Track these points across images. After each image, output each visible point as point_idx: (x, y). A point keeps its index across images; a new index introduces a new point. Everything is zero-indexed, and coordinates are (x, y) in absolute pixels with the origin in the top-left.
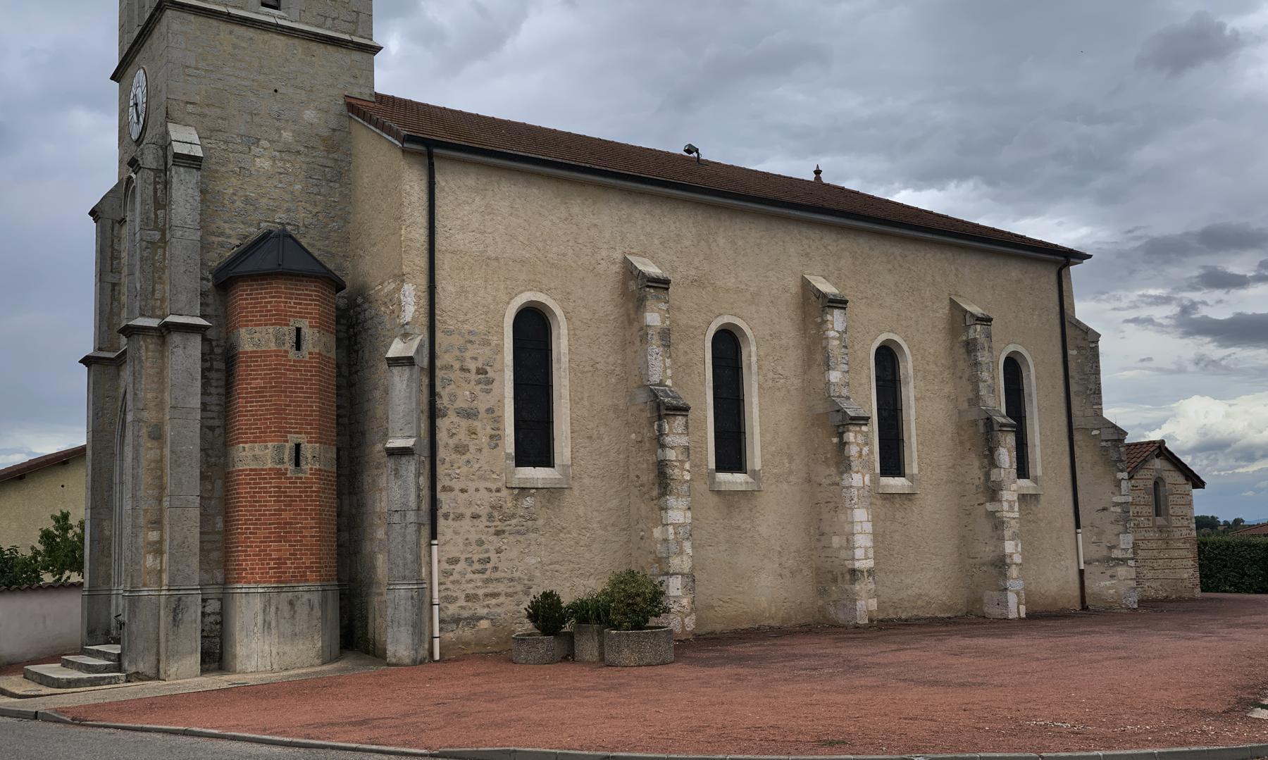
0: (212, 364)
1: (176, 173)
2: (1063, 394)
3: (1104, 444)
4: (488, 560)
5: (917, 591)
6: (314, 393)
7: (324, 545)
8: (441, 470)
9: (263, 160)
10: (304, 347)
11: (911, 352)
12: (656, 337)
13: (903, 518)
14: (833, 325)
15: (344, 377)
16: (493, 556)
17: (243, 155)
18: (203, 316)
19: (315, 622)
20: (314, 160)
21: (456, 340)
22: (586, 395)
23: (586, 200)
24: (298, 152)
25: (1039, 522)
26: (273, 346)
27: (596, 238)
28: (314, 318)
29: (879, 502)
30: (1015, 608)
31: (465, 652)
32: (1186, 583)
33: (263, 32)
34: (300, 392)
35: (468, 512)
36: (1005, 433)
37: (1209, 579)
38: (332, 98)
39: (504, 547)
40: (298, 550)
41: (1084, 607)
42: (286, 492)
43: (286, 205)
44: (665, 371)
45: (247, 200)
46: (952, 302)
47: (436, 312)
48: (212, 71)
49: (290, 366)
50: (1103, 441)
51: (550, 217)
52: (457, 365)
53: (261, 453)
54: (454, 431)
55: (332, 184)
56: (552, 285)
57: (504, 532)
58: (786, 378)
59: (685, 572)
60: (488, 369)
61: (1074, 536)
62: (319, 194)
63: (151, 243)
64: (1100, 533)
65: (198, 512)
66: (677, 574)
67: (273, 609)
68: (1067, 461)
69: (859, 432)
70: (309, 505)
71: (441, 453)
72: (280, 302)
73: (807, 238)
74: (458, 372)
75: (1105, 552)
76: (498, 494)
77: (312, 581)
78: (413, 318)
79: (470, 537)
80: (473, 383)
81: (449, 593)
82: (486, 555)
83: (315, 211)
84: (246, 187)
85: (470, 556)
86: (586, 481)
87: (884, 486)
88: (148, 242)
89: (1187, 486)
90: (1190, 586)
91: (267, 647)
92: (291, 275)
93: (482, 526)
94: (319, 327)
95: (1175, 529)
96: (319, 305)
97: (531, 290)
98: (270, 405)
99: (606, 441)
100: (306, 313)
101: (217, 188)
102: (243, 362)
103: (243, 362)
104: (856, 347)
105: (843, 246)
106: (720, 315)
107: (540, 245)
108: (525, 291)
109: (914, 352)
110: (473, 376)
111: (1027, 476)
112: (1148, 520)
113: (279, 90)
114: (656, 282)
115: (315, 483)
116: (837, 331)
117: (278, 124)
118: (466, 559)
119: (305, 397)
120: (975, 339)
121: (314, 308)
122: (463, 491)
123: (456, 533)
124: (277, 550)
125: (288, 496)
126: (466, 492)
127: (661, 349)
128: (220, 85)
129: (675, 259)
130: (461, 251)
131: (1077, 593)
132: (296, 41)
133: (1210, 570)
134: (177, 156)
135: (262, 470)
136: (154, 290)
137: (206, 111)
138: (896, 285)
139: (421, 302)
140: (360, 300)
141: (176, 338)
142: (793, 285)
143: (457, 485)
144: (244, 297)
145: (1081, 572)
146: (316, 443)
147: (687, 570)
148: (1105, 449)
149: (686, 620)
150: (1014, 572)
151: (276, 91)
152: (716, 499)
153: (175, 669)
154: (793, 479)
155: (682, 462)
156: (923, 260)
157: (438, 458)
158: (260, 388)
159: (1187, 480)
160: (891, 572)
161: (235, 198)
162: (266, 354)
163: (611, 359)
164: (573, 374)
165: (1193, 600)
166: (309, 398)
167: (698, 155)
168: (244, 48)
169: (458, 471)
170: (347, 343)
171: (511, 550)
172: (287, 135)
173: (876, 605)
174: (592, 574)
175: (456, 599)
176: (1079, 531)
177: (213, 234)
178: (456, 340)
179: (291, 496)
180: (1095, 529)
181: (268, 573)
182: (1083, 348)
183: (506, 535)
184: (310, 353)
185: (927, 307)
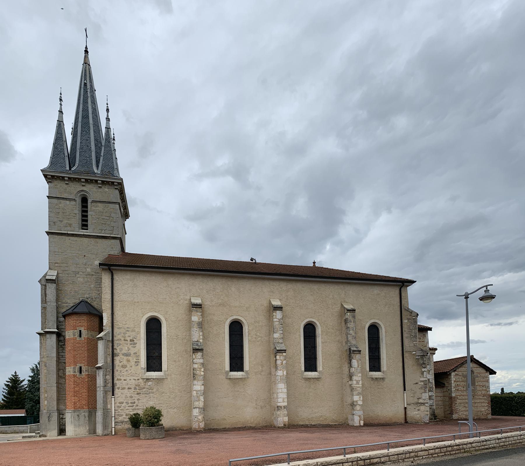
1: (48, 285)
2: (400, 338)
3: (417, 357)
4: (134, 403)
5: (320, 414)
7: (90, 398)
8: (116, 373)
9: (80, 278)
11: (321, 325)
12: (196, 325)
13: (314, 387)
14: (276, 317)
16: (136, 401)
19: (86, 422)
20: (98, 277)
21: (123, 331)
22: (173, 347)
23: (175, 279)
24: (93, 275)
25: (384, 389)
26: (72, 337)
27: (179, 292)
28: (85, 327)
29: (303, 381)
30: (357, 421)
32: (484, 413)
33: (81, 238)
34: (81, 350)
35: (127, 387)
36: (356, 354)
37: (517, 411)
38: (104, 256)
39: (140, 399)
40: (81, 399)
41: (406, 422)
42: (76, 382)
43: (88, 292)
44: (199, 337)
45: (75, 292)
48: (63, 252)
49: (77, 342)
50: (417, 356)
51: (160, 286)
52: (123, 339)
54: (121, 361)
56: (160, 310)
57: (140, 393)
58: (261, 337)
59: (200, 407)
60: (134, 339)
61: (403, 394)
64: (415, 393)
65: (55, 388)
66: (197, 408)
68: (401, 364)
69: (281, 355)
70: (84, 386)
71: (117, 368)
72: (74, 322)
73: (272, 285)
74: (123, 341)
75: (416, 400)
76: (138, 381)
77: (85, 409)
78: (106, 324)
81: (120, 413)
82: (134, 401)
84: (75, 287)
85: (127, 401)
86: (173, 376)
87: (230, 376)
88: (43, 307)
89: (486, 374)
90: (486, 414)
91: (72, 428)
92: (76, 313)
93: (132, 391)
95: (478, 391)
96: (87, 323)
97: (152, 312)
99: (181, 362)
100: (82, 325)
101: (65, 289)
104: (294, 325)
105: (289, 287)
106: (232, 316)
107: (156, 296)
108: (149, 312)
109: (322, 325)
110: (129, 342)
111: (379, 370)
112: (464, 387)
113: (86, 256)
114: (197, 306)
115: (86, 379)
116: (278, 319)
117: (85, 266)
119: (83, 352)
120: (347, 318)
121: (85, 324)
122: (124, 380)
124: (74, 399)
125: (77, 383)
126: (126, 380)
127: (198, 329)
128: (66, 256)
129: (212, 297)
130: (124, 301)
131: (403, 416)
132: (92, 239)
133: (517, 407)
135: (71, 375)
136: (45, 322)
137: (62, 265)
138: (315, 300)
139: (109, 319)
142: (266, 303)
143: (122, 378)
145: (405, 408)
146: (86, 366)
147: (201, 407)
148: (418, 359)
149: (200, 424)
150: (358, 408)
151: (85, 256)
152: (228, 381)
154: (263, 373)
155: (200, 368)
156: (328, 290)
159: (486, 371)
160: (308, 407)
161: (71, 291)
163: (184, 334)
164: (168, 340)
165: (486, 419)
166: (84, 352)
167: (255, 261)
168: (74, 243)
169: (123, 374)
171: (143, 400)
172: (89, 270)
173: (287, 419)
174: (175, 408)
175: (122, 415)
176: (405, 392)
177: (64, 303)
178: (123, 331)
179: (78, 383)
180: (413, 391)
182: (410, 319)
183: (141, 394)
185: (329, 307)
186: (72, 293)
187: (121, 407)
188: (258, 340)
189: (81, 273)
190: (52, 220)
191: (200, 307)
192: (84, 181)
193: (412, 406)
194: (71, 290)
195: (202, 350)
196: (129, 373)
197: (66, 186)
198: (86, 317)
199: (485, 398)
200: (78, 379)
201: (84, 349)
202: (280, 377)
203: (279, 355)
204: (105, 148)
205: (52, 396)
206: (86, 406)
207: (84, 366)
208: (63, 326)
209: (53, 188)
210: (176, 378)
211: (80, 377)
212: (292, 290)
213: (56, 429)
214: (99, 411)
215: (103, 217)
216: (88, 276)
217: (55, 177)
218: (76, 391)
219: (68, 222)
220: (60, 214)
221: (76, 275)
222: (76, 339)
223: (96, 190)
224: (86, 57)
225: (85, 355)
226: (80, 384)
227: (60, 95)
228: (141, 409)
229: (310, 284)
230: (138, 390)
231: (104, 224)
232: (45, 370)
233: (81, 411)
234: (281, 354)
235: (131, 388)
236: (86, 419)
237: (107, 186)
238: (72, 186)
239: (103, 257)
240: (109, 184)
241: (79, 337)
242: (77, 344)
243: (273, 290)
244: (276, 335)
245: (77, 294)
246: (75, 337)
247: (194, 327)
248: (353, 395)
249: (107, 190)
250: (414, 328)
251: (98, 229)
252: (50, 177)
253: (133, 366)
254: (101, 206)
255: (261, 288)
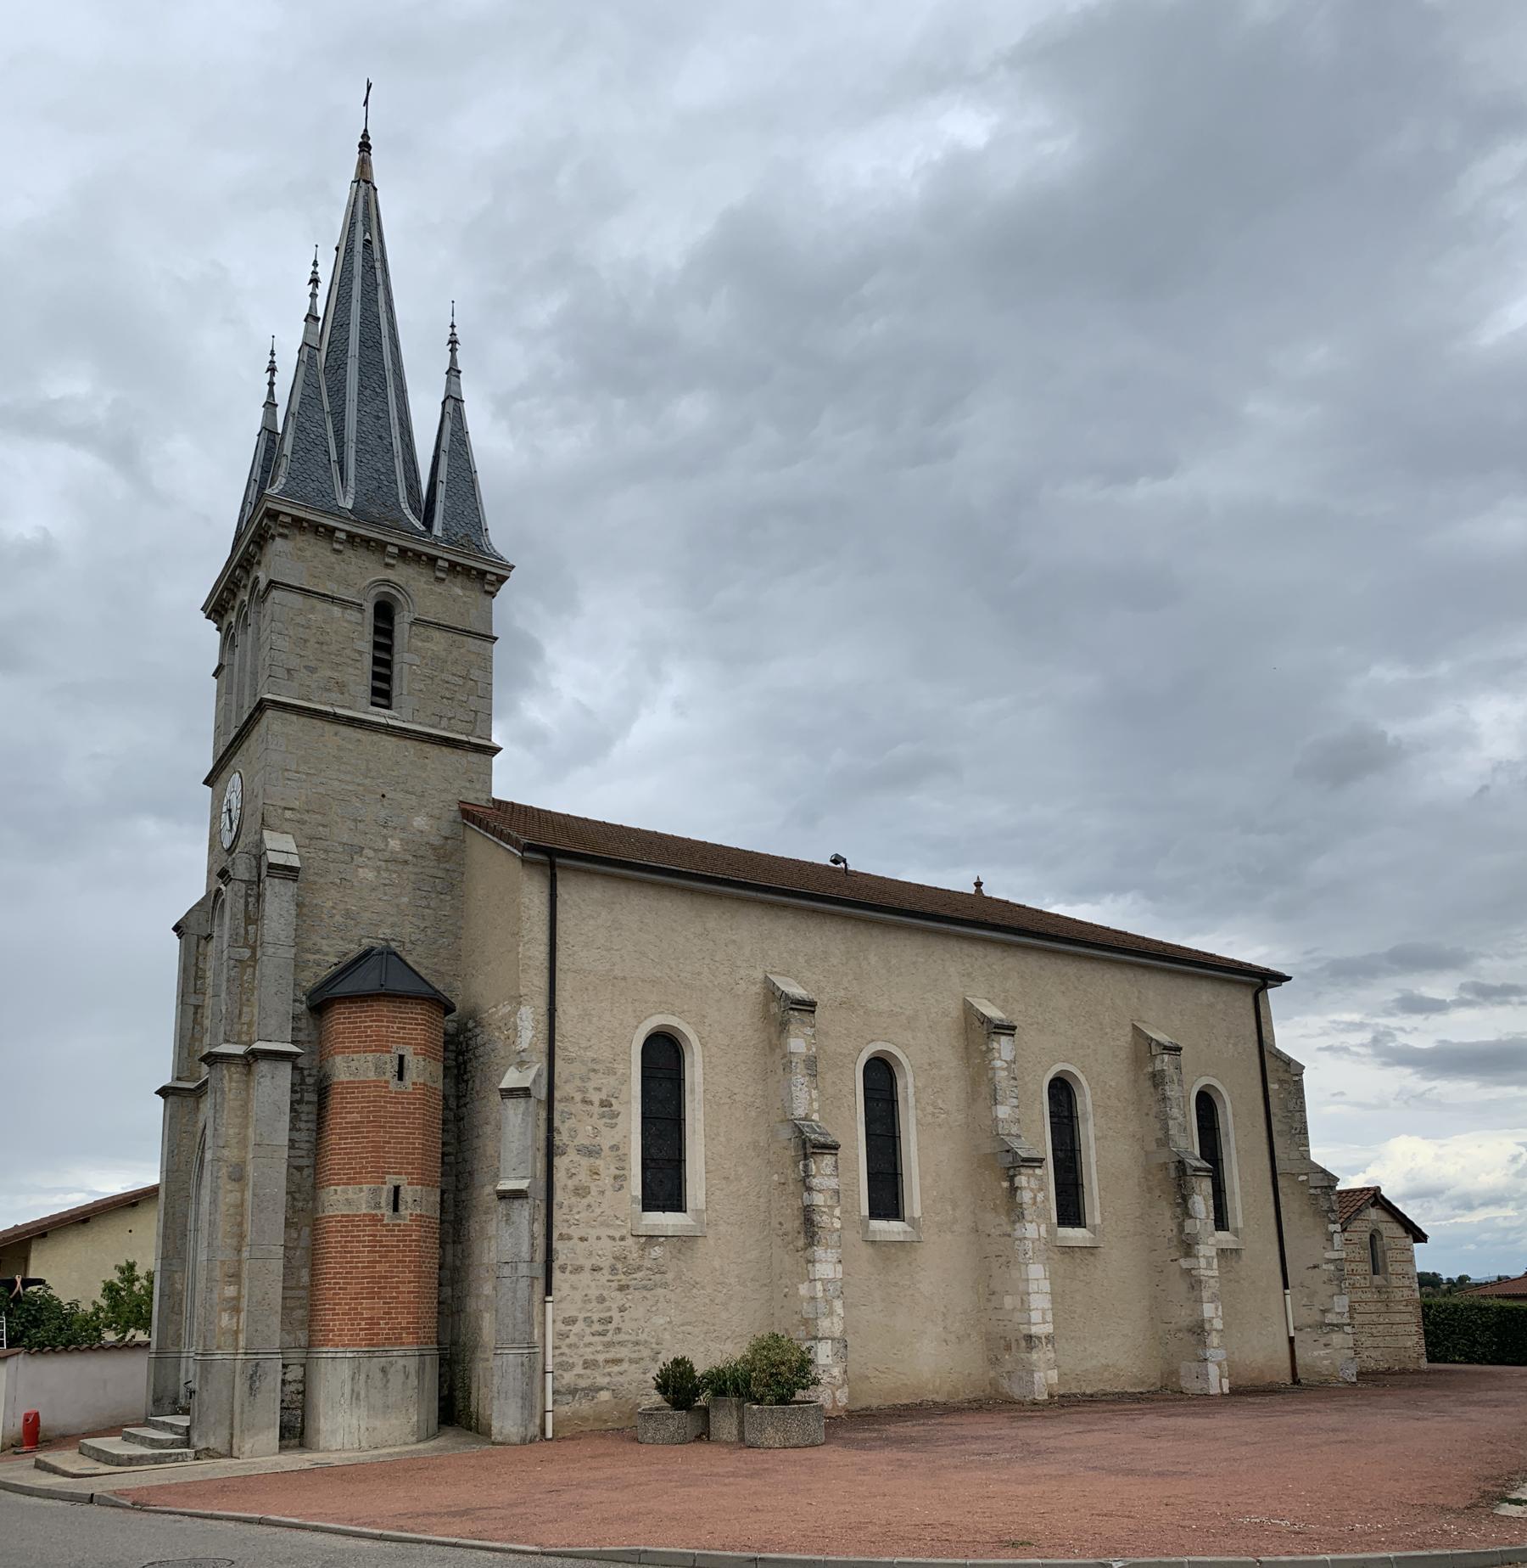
0: (302, 1096)
2: (1264, 1134)
4: (610, 1320)
5: (1104, 1361)
6: (417, 1129)
8: (558, 1215)
10: (407, 1076)
12: (801, 1066)
14: (1000, 1053)
15: (451, 1110)
17: (345, 866)
18: (294, 1042)
20: (423, 870)
24: (406, 862)
25: (1242, 1282)
26: (372, 1076)
28: (419, 1044)
30: (1217, 1382)
31: (581, 1429)
34: (402, 1128)
35: (588, 1264)
40: (393, 1308)
45: (348, 914)
46: (1135, 1027)
47: (557, 1037)
49: (391, 1097)
50: (1311, 1187)
52: (578, 1097)
53: (356, 1196)
54: (573, 1171)
55: (442, 896)
56: (686, 1007)
57: (628, 1286)
58: (947, 1113)
59: (836, 1336)
60: (613, 1101)
61: (1282, 1297)
62: (428, 907)
63: (240, 961)
66: (827, 1338)
67: (363, 1377)
70: (407, 1256)
71: (559, 1196)
72: (382, 1026)
74: (579, 1104)
75: (1318, 1317)
76: (622, 1243)
77: (408, 1344)
79: (589, 1292)
80: (596, 1116)
81: (564, 1358)
82: (608, 1314)
83: (422, 926)
84: (346, 899)
85: (589, 1314)
86: (722, 1228)
90: (1415, 1355)
94: (424, 1054)
95: (1396, 1290)
97: (662, 1013)
98: (367, 1142)
99: (745, 1183)
100: (410, 1039)
101: (315, 902)
102: (337, 1093)
103: (337, 1093)
104: (1027, 1079)
107: (673, 963)
110: (596, 1109)
111: (1223, 1226)
112: (1365, 1279)
115: (415, 1231)
118: (585, 1319)
119: (407, 1133)
121: (419, 1034)
122: (582, 1239)
123: (574, 1288)
127: (807, 1078)
128: (321, 790)
129: (821, 978)
132: (408, 743)
134: (271, 866)
137: (306, 817)
139: (540, 1026)
140: (471, 1024)
141: (263, 1067)
142: (955, 1010)
143: (573, 1231)
144: (341, 1020)
145: (1291, 1340)
149: (838, 1394)
150: (1214, 1339)
151: (383, 796)
153: (250, 1445)
157: (555, 1202)
158: (357, 1122)
159: (1406, 1232)
161: (334, 911)
162: (365, 1084)
163: (751, 1090)
166: (411, 1133)
169: (577, 1217)
170: (456, 1071)
172: (394, 844)
175: (573, 1366)
176: (1288, 1291)
177: (308, 951)
181: (358, 1335)
182: (1285, 1082)
184: (414, 1084)
186: (337, 918)
187: (568, 1337)
188: (939, 1120)
189: (371, 853)
190: (282, 660)
191: (812, 1009)
192: (397, 551)
193: (1307, 1332)
194: (333, 908)
195: (836, 1147)
196: (595, 1215)
197: (333, 558)
198: (421, 1009)
199: (1410, 1308)
200: (387, 1231)
201: (412, 1123)
202: (1033, 1243)
203: (1025, 1175)
204: (449, 459)
205: (267, 1296)
206: (412, 1333)
207: (409, 1184)
208: (301, 1034)
209: (289, 556)
210: (731, 1235)
211: (394, 1225)
212: (1015, 974)
213: (275, 1424)
214: (506, 1352)
215: (445, 676)
216: (391, 866)
217: (305, 524)
218: (379, 1277)
219: (335, 675)
220: (308, 644)
221: (352, 858)
222: (387, 1087)
223: (426, 586)
224: (364, 166)
225: (414, 1144)
226: (393, 1251)
227: (312, 268)
228: (628, 1341)
229: (1059, 961)
230: (623, 1277)
231: (448, 699)
232: (229, 1195)
233: (395, 1353)
234: (1030, 1171)
235: (601, 1269)
236: (409, 1381)
237: (460, 578)
238: (354, 560)
239: (441, 805)
240: (316, 532)
241: (396, 1078)
242: (391, 1102)
243: (971, 969)
244: (1003, 1112)
245: (352, 922)
246: (386, 1078)
247: (798, 1071)
248: (1199, 1301)
249: (460, 592)
250: (1297, 1109)
251: (429, 713)
252: (288, 520)
253: (607, 1193)
254: (438, 642)
255: (940, 962)
